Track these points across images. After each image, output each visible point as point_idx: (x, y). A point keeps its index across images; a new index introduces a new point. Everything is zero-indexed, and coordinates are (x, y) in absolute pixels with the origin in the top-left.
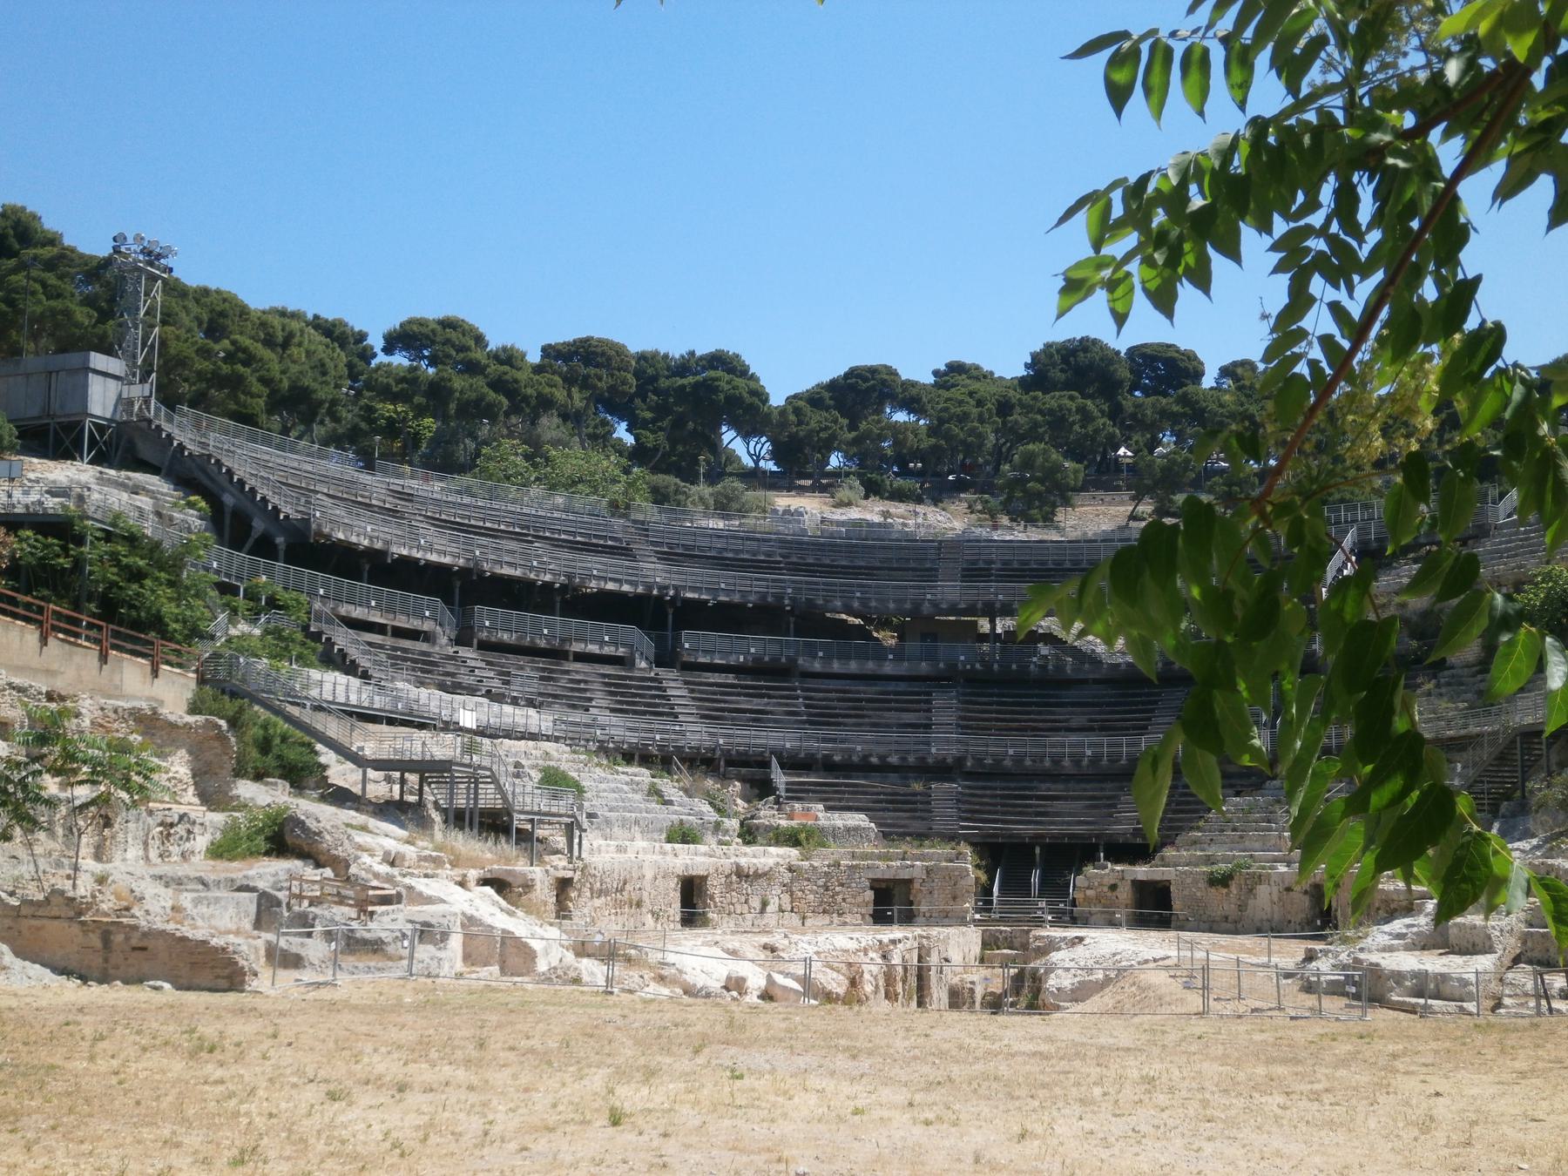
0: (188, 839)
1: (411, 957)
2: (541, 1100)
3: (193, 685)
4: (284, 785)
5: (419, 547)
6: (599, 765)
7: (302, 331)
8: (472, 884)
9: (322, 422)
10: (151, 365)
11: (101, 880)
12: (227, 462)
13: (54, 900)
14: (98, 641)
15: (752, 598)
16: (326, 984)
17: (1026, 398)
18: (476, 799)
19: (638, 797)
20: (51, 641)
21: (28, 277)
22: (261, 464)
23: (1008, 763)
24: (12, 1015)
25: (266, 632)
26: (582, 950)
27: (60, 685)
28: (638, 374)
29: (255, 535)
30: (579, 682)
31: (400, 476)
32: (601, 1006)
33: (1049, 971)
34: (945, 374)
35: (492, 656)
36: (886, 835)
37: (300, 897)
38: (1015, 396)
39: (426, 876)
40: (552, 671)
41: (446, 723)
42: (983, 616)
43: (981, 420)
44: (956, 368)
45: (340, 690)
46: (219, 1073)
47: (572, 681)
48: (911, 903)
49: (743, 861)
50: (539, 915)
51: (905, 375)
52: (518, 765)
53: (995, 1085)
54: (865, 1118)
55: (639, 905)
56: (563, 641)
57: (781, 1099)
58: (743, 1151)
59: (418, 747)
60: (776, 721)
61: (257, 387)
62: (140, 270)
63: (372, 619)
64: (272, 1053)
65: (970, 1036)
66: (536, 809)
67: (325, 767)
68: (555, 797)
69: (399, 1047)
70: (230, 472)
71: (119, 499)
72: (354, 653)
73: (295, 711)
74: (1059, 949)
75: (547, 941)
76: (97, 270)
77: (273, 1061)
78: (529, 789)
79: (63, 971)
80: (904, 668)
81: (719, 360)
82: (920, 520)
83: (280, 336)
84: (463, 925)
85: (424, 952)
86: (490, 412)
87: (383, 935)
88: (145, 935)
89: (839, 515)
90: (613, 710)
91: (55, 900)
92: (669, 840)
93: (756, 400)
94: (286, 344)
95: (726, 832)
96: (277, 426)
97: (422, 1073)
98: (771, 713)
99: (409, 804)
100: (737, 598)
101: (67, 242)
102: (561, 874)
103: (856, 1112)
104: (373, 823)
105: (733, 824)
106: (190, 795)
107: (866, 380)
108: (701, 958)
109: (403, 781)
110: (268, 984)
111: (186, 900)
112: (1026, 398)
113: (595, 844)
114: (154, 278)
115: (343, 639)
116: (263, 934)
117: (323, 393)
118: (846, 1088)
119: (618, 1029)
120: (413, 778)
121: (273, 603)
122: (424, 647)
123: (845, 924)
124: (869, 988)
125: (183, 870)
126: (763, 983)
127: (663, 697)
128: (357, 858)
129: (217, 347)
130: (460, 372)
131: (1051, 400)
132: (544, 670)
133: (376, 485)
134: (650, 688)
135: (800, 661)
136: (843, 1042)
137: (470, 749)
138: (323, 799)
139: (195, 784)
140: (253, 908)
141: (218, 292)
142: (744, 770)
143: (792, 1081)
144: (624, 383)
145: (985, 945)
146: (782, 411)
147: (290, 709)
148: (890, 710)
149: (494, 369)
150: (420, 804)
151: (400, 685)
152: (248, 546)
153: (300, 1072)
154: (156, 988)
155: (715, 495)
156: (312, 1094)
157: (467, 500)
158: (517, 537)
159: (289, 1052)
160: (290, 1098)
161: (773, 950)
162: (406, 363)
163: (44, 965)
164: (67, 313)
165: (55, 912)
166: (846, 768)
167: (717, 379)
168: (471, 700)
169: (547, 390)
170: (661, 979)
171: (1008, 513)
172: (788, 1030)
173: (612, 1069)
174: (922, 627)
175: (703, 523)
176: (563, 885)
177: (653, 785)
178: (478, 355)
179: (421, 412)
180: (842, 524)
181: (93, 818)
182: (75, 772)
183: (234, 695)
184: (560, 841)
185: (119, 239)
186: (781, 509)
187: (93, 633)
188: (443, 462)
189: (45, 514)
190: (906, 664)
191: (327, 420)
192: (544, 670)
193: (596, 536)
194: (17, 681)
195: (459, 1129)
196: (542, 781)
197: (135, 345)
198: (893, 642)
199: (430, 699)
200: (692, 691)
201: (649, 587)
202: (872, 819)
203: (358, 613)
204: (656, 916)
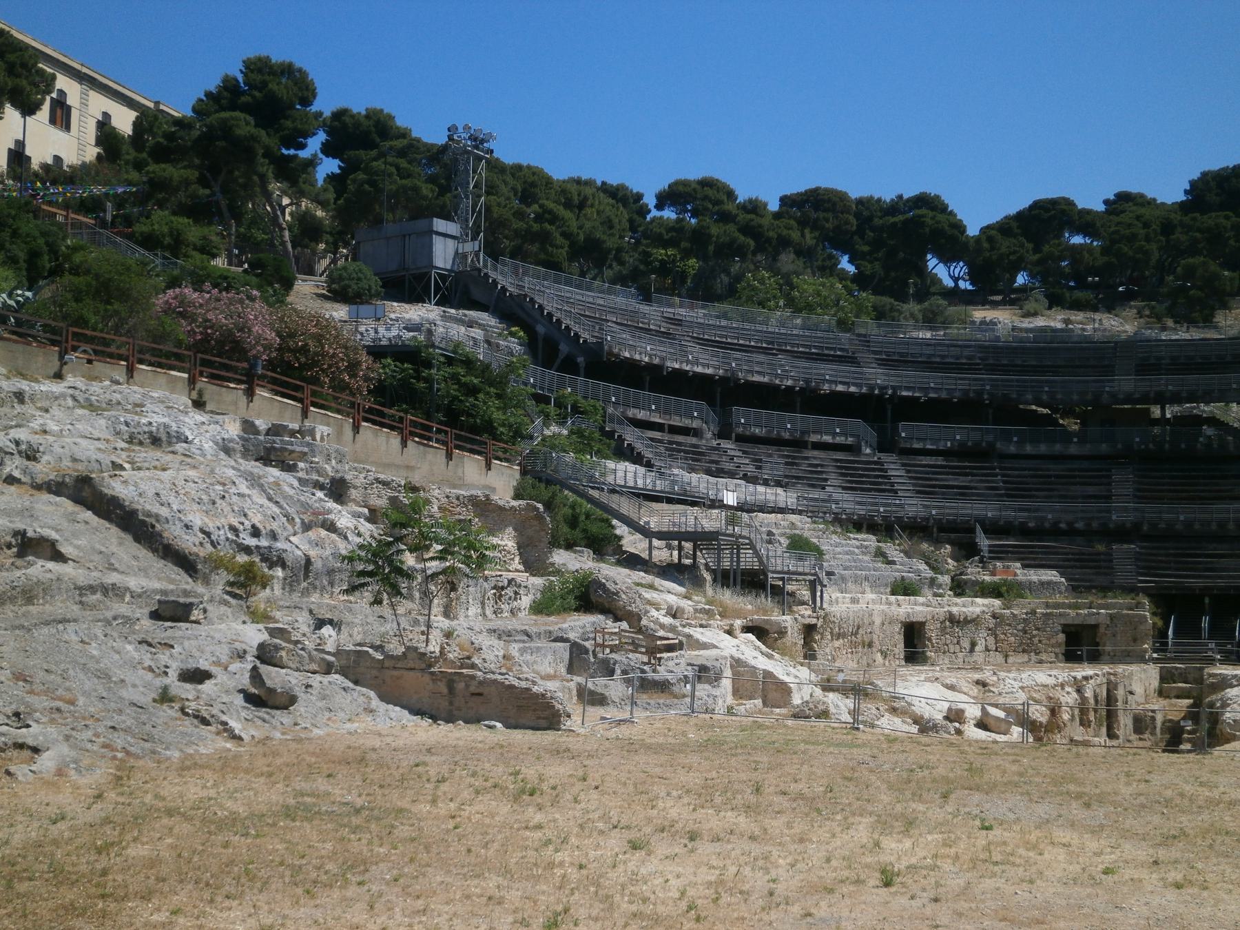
0: (515, 599)
1: (693, 696)
2: (815, 852)
3: (518, 476)
4: (588, 552)
5: (688, 362)
6: (835, 532)
7: (594, 196)
8: (738, 632)
9: (610, 267)
10: (479, 227)
11: (448, 635)
12: (539, 300)
13: (410, 656)
14: (444, 443)
15: (957, 394)
16: (624, 721)
17: (1187, 219)
18: (738, 562)
19: (867, 558)
20: (410, 443)
21: (385, 163)
22: (564, 300)
23: (1179, 527)
24: (374, 756)
25: (571, 432)
26: (827, 686)
27: (416, 479)
28: (857, 215)
29: (561, 356)
30: (817, 466)
31: (671, 305)
32: (852, 745)
33: (1225, 705)
34: (1114, 202)
35: (748, 447)
36: (1075, 589)
37: (603, 646)
38: (1176, 217)
39: (701, 626)
40: (795, 458)
41: (712, 501)
42: (1155, 403)
43: (1148, 239)
44: (1123, 197)
45: (630, 476)
46: (539, 818)
48: (1097, 644)
49: (955, 610)
50: (792, 657)
51: (1081, 204)
52: (770, 533)
53: (1228, 840)
54: (1116, 877)
55: (870, 645)
56: (803, 433)
57: (1031, 854)
59: (692, 521)
60: (978, 495)
61: (560, 240)
62: (468, 152)
63: (652, 419)
64: (582, 796)
65: (1187, 782)
66: (786, 569)
67: (620, 538)
68: (801, 559)
69: (688, 791)
70: (541, 308)
71: (458, 332)
72: (639, 446)
73: (595, 494)
74: (1232, 686)
75: (798, 678)
76: (437, 155)
77: (583, 805)
78: (779, 553)
79: (417, 712)
80: (1087, 449)
81: (925, 202)
82: (1097, 325)
83: (576, 200)
84: (732, 666)
85: (703, 690)
86: (741, 252)
87: (669, 677)
88: (481, 683)
89: (1026, 323)
90: (844, 488)
91: (411, 655)
93: (956, 232)
94: (582, 206)
95: (940, 586)
96: (577, 271)
97: (711, 820)
98: (975, 488)
99: (686, 566)
100: (944, 395)
101: (414, 134)
102: (808, 621)
104: (658, 582)
105: (945, 579)
106: (516, 563)
107: (1047, 210)
108: (926, 691)
109: (680, 548)
110: (581, 722)
111: (514, 649)
112: (1187, 219)
114: (480, 158)
115: (631, 436)
116: (575, 678)
117: (611, 243)
118: (1093, 845)
120: (688, 546)
121: (576, 410)
122: (694, 440)
123: (1041, 662)
124: (1066, 717)
125: (513, 624)
126: (978, 714)
127: (885, 477)
128: (647, 612)
129: (529, 210)
130: (716, 221)
131: (1208, 220)
132: (788, 457)
133: (653, 313)
134: (874, 470)
135: (998, 445)
136: (1072, 787)
137: (732, 521)
138: (619, 563)
139: (520, 554)
140: (567, 656)
141: (529, 167)
142: (953, 536)
143: (1037, 833)
144: (847, 223)
145: (1163, 679)
146: (977, 240)
147: (591, 492)
148: (1075, 484)
149: (742, 217)
150: (694, 566)
151: (676, 471)
152: (556, 365)
153: (605, 817)
154: (490, 727)
155: (924, 311)
156: (615, 843)
157: (724, 323)
159: (594, 795)
160: (598, 846)
161: (984, 685)
162: (673, 216)
163: (403, 707)
164: (416, 189)
165: (411, 665)
166: (1038, 533)
167: (923, 216)
168: (732, 482)
169: (785, 232)
170: (894, 710)
171: (1172, 317)
172: (1021, 775)
174: (1101, 415)
175: (915, 334)
176: (809, 630)
177: (879, 548)
178: (729, 207)
179: (686, 254)
180: (1027, 330)
181: (443, 583)
182: (427, 548)
183: (549, 482)
184: (805, 594)
185: (452, 129)
186: (978, 320)
187: (440, 437)
188: (703, 292)
189: (404, 345)
190: (1088, 446)
191: (614, 264)
192: (788, 457)
193: (827, 348)
194: (382, 477)
195: (746, 887)
197: (467, 211)
198: (1076, 427)
199: (699, 482)
200: (908, 471)
201: (872, 388)
202: (1062, 575)
203: (641, 415)
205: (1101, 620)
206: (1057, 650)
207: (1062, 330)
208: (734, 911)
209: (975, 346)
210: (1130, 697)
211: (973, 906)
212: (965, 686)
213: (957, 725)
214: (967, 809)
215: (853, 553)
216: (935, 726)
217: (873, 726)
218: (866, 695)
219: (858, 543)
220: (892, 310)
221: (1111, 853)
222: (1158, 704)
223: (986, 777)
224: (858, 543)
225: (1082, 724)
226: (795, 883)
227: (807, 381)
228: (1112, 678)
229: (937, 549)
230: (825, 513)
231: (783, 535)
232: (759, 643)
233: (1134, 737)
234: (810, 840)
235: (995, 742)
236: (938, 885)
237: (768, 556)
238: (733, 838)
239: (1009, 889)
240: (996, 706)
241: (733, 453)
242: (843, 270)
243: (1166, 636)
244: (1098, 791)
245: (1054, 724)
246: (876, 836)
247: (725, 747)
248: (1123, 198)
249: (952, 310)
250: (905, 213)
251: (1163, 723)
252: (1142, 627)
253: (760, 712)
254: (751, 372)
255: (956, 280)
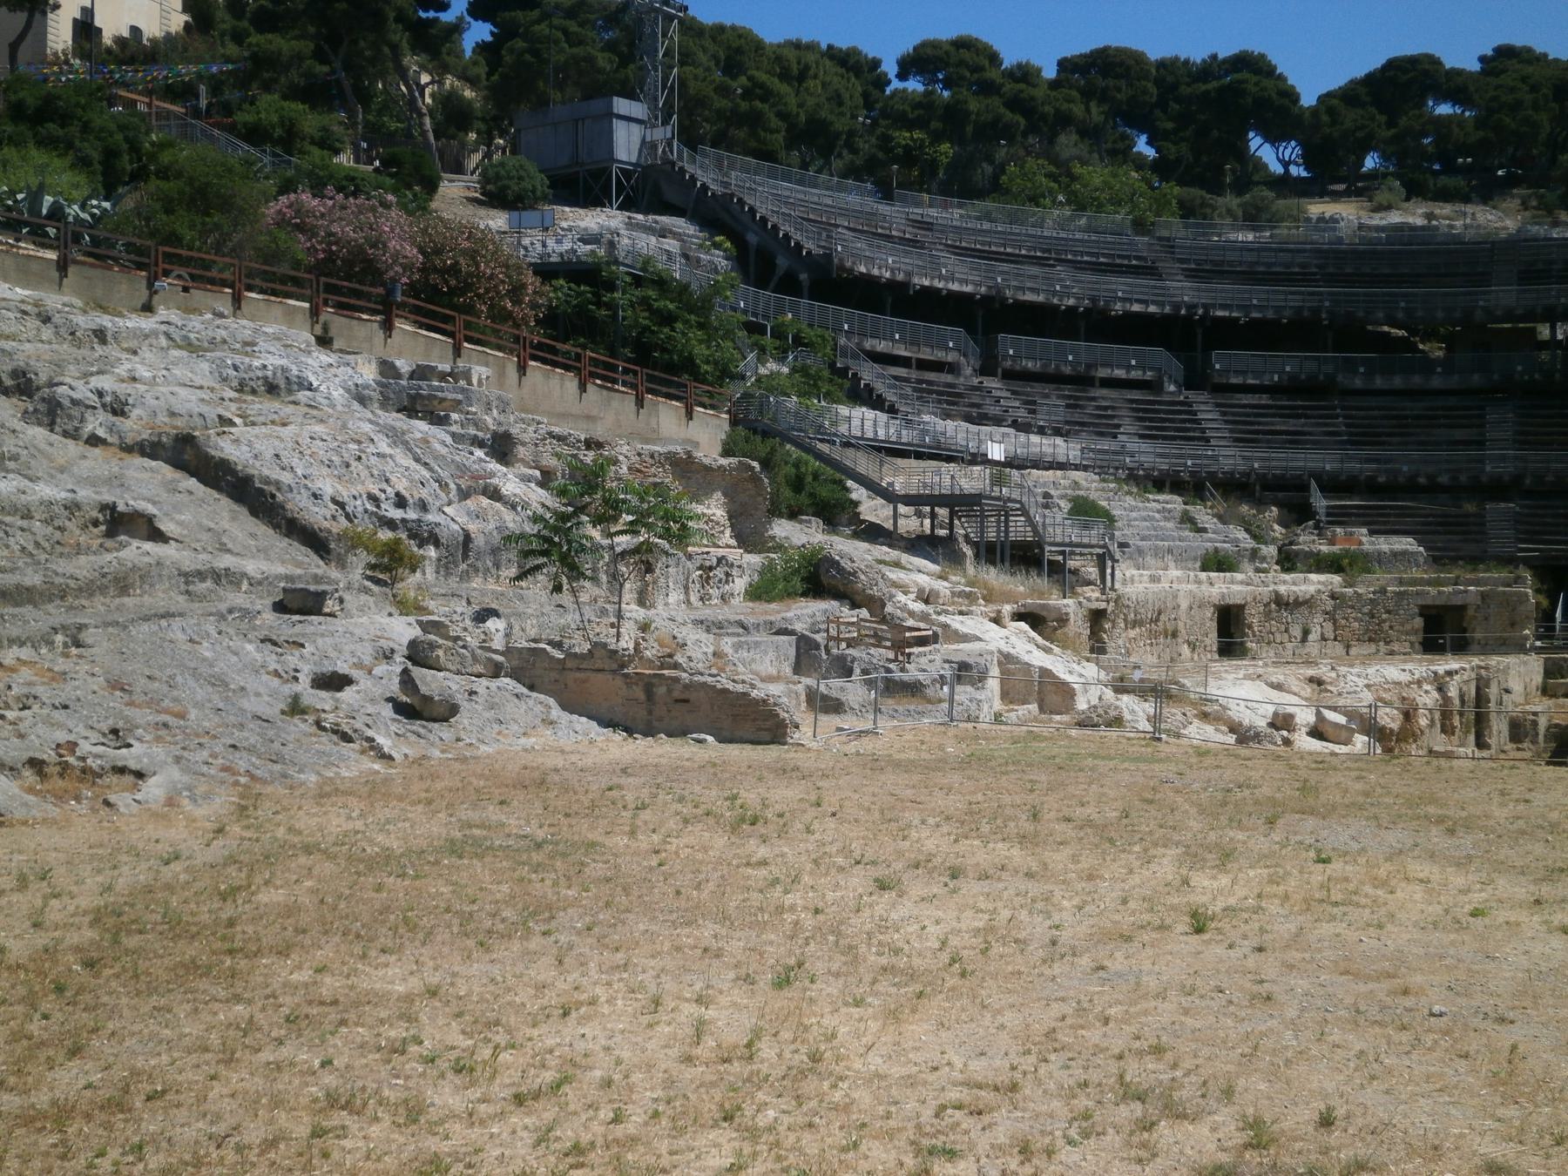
2: (1108, 893)
6: (1129, 493)
8: (1007, 620)
15: (1287, 313)
18: (1007, 532)
19: (1170, 525)
26: (1121, 687)
28: (1159, 82)
30: (1106, 408)
35: (1017, 386)
36: (1436, 560)
42: (1543, 321)
47: (1099, 408)
49: (1282, 589)
50: (1076, 651)
52: (1047, 495)
54: (1487, 921)
55: (1175, 635)
56: (1089, 366)
57: (1380, 892)
58: (1357, 975)
66: (1067, 540)
68: (1086, 527)
78: (1059, 520)
82: (1468, 221)
84: (1000, 663)
89: (1377, 220)
90: (1142, 436)
92: (1204, 569)
93: (1286, 101)
95: (1263, 559)
98: (1310, 434)
100: (1270, 315)
103: (1475, 914)
105: (1270, 551)
108: (1245, 692)
113: (1128, 574)
118: (1459, 880)
119: (1178, 791)
123: (1392, 653)
124: (1423, 722)
126: (1312, 719)
132: (1069, 397)
135: (1340, 378)
136: (1431, 810)
137: (998, 481)
142: (1280, 495)
145: (1548, 673)
146: (1314, 111)
157: (986, 226)
158: (1038, 261)
169: (1065, 106)
170: (1204, 716)
172: (1367, 794)
173: (1180, 850)
175: (1232, 236)
177: (1186, 512)
180: (1379, 229)
184: (1092, 571)
192: (1069, 397)
193: (1120, 256)
196: (1073, 512)
198: (1440, 354)
200: (1224, 414)
202: (1420, 543)
204: (1193, 646)
205: (1471, 600)
206: (1413, 638)
207: (1423, 228)
208: (1007, 963)
209: (1311, 251)
210: (1505, 697)
211: (1307, 956)
212: (1295, 685)
213: (1285, 733)
214: (1299, 838)
215: (1152, 519)
216: (1257, 735)
217: (1178, 736)
218: (1170, 697)
219: (1159, 506)
220: (1203, 204)
221: (1481, 891)
222: (1541, 705)
223: (1323, 797)
224: (1159, 506)
225: (1443, 731)
226: (1083, 930)
227: (1094, 300)
228: (1483, 672)
229: (1259, 512)
230: (1117, 469)
231: (1062, 497)
232: (1033, 634)
233: (1510, 746)
234: (1102, 878)
235: (1333, 754)
236: (1262, 931)
237: (1044, 524)
238: (1004, 875)
239: (1352, 936)
240: (1334, 709)
241: (999, 394)
242: (1140, 153)
243: (1553, 619)
244: (1464, 814)
245: (1408, 732)
246: (1184, 872)
247: (993, 763)
248: (1505, 53)
249: (1281, 204)
250: (1220, 78)
251: (1548, 729)
252: (1522, 608)
253: (1036, 719)
254: (1022, 289)
255: (1286, 164)
